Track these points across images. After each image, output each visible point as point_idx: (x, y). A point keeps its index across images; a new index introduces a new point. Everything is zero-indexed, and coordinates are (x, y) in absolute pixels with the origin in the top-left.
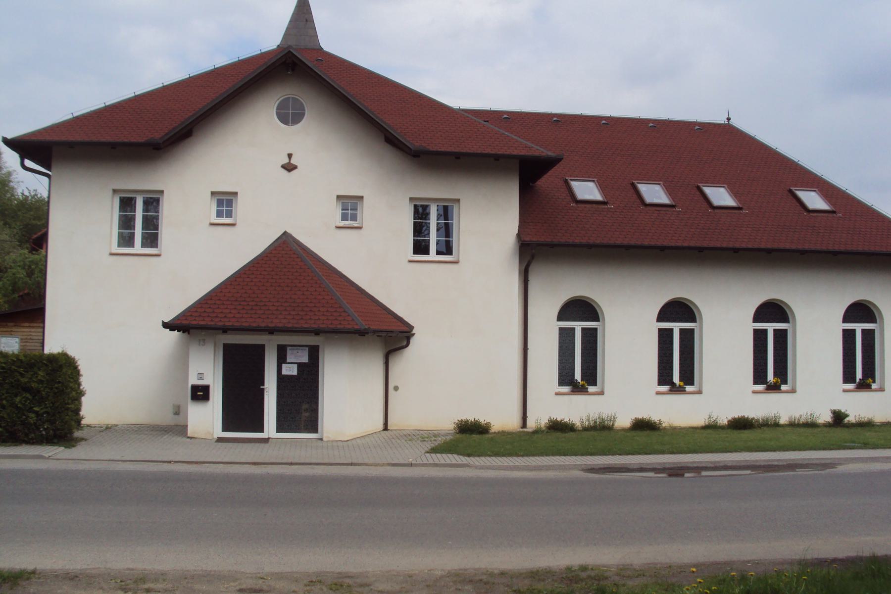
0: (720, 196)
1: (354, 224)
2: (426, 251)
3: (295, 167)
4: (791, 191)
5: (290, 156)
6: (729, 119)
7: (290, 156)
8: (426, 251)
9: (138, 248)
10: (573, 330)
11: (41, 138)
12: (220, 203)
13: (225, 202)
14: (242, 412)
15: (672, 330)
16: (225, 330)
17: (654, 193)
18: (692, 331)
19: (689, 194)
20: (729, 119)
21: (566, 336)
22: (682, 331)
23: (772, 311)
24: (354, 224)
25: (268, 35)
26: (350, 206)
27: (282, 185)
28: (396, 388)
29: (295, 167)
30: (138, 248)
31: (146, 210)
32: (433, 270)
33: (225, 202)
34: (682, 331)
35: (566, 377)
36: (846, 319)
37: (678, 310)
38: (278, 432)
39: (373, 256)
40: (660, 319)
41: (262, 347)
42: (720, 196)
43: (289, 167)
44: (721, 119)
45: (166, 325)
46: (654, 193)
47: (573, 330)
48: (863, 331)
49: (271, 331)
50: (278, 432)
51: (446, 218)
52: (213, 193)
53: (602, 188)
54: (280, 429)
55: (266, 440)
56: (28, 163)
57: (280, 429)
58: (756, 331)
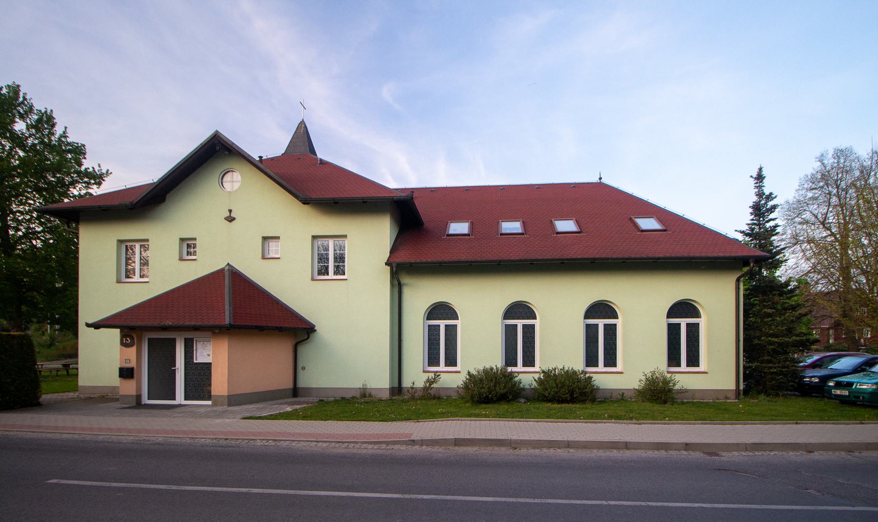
3: (234, 219)
4: (631, 219)
5: (230, 211)
6: (600, 179)
7: (230, 211)
13: (188, 246)
15: (516, 325)
18: (533, 326)
20: (600, 179)
21: (433, 332)
22: (524, 326)
23: (441, 310)
27: (244, 231)
28: (303, 368)
29: (234, 219)
31: (327, 268)
34: (524, 326)
35: (433, 360)
39: (287, 278)
40: (670, 315)
41: (174, 340)
43: (230, 219)
44: (595, 179)
48: (688, 325)
53: (578, 223)
54: (187, 398)
55: (180, 406)
57: (187, 398)
58: (669, 325)
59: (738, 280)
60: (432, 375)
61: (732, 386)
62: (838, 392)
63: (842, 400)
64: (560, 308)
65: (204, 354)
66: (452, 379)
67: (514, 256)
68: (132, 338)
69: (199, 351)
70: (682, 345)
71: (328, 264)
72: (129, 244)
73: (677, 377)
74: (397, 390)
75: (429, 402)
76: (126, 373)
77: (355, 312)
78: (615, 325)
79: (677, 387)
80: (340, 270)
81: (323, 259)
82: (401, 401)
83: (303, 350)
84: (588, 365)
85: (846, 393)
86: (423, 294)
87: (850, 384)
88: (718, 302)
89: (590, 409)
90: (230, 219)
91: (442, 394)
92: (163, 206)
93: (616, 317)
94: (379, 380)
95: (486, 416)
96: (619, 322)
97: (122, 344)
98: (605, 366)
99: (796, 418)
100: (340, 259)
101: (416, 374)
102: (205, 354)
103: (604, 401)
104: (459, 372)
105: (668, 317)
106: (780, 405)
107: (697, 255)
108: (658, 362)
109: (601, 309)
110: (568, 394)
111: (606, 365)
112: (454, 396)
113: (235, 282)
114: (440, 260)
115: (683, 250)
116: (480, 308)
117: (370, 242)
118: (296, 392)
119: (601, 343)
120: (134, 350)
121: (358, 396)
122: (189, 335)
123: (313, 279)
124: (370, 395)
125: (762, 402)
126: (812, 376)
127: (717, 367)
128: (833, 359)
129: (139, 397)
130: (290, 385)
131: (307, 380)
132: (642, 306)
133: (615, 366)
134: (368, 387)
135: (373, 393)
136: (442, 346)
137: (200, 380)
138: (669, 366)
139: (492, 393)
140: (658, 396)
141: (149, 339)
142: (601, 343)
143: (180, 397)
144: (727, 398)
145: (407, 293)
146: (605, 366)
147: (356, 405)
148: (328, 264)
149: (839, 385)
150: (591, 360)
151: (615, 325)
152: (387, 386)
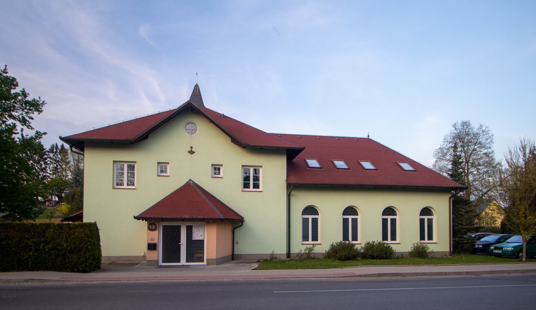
0: (367, 165)
1: (219, 176)
2: (122, 184)
3: (194, 152)
4: (358, 162)
5: (191, 147)
6: (368, 136)
7: (191, 147)
8: (122, 184)
9: (251, 188)
10: (387, 219)
11: (75, 137)
12: (215, 169)
13: (162, 167)
14: (171, 253)
16: (163, 220)
17: (340, 164)
18: (432, 219)
19: (354, 165)
20: (368, 136)
21: (305, 222)
23: (311, 210)
24: (219, 176)
25: (183, 97)
26: (217, 169)
27: (195, 160)
28: (237, 243)
29: (194, 152)
30: (251, 188)
32: (251, 195)
33: (162, 167)
35: (305, 237)
36: (421, 214)
37: (389, 211)
38: (187, 262)
39: (227, 189)
40: (344, 214)
42: (367, 165)
43: (191, 152)
44: (366, 136)
45: (135, 218)
46: (340, 164)
47: (387, 219)
48: (312, 219)
49: (183, 220)
50: (187, 262)
51: (256, 174)
52: (158, 163)
53: (319, 162)
55: (183, 266)
56: (74, 149)
58: (383, 219)
59: (450, 198)
60: (311, 246)
61: (448, 250)
62: (497, 251)
63: (498, 255)
64: (370, 209)
65: (197, 235)
66: (323, 246)
67: (353, 183)
68: (155, 225)
69: (195, 233)
70: (426, 230)
71: (251, 181)
72: (217, 167)
73: (429, 245)
74: (289, 255)
75: (308, 259)
76: (152, 247)
77: (268, 211)
78: (317, 219)
79: (429, 250)
80: (256, 186)
81: (247, 179)
82: (291, 260)
83: (236, 231)
84: (383, 240)
85: (501, 252)
86: (302, 200)
87: (502, 248)
88: (441, 207)
89: (426, 260)
90: (191, 152)
91: (316, 256)
92: (146, 140)
93: (318, 214)
94: (282, 250)
95: (352, 265)
96: (359, 217)
97: (149, 229)
98: (428, 240)
99: (482, 262)
100: (256, 179)
101: (299, 247)
102: (199, 235)
103: (398, 258)
104: (320, 244)
105: (420, 215)
106: (464, 257)
107: (420, 185)
108: (415, 239)
109: (350, 211)
110: (379, 254)
111: (391, 240)
112: (321, 257)
113: (191, 191)
114: (316, 183)
115: (415, 181)
116: (330, 208)
117: (274, 171)
118: (233, 257)
119: (389, 228)
120: (156, 232)
121: (269, 259)
122: (189, 224)
123: (113, 188)
124: (276, 258)
125: (457, 257)
126: (479, 245)
127: (441, 241)
128: (484, 236)
129: (157, 261)
130: (231, 253)
131: (240, 250)
132: (408, 209)
133: (317, 240)
134: (275, 253)
135: (278, 257)
136: (311, 230)
137: (196, 249)
138: (303, 241)
139: (343, 254)
140: (420, 254)
141: (164, 227)
142: (389, 228)
143: (183, 261)
144: (445, 256)
145: (292, 198)
146: (428, 240)
147: (269, 262)
148: (251, 181)
149: (496, 248)
150: (385, 237)
151: (317, 219)
152: (285, 253)
